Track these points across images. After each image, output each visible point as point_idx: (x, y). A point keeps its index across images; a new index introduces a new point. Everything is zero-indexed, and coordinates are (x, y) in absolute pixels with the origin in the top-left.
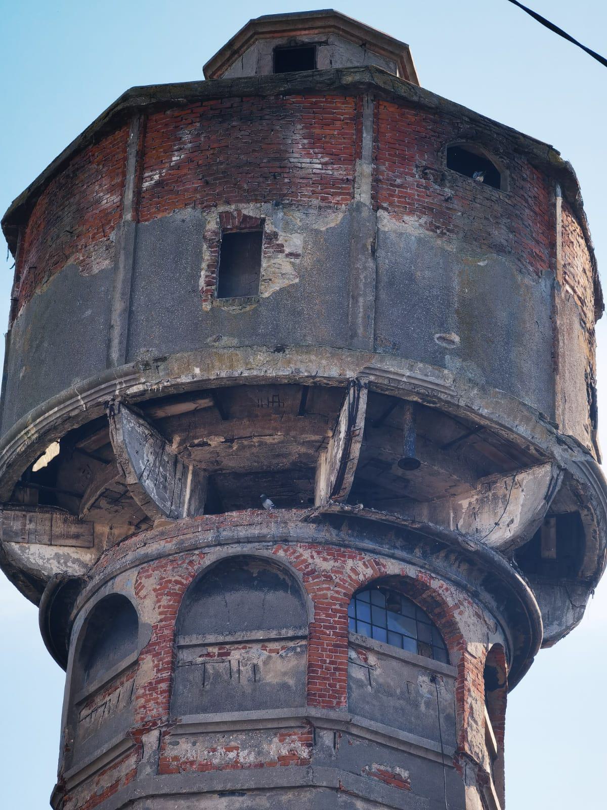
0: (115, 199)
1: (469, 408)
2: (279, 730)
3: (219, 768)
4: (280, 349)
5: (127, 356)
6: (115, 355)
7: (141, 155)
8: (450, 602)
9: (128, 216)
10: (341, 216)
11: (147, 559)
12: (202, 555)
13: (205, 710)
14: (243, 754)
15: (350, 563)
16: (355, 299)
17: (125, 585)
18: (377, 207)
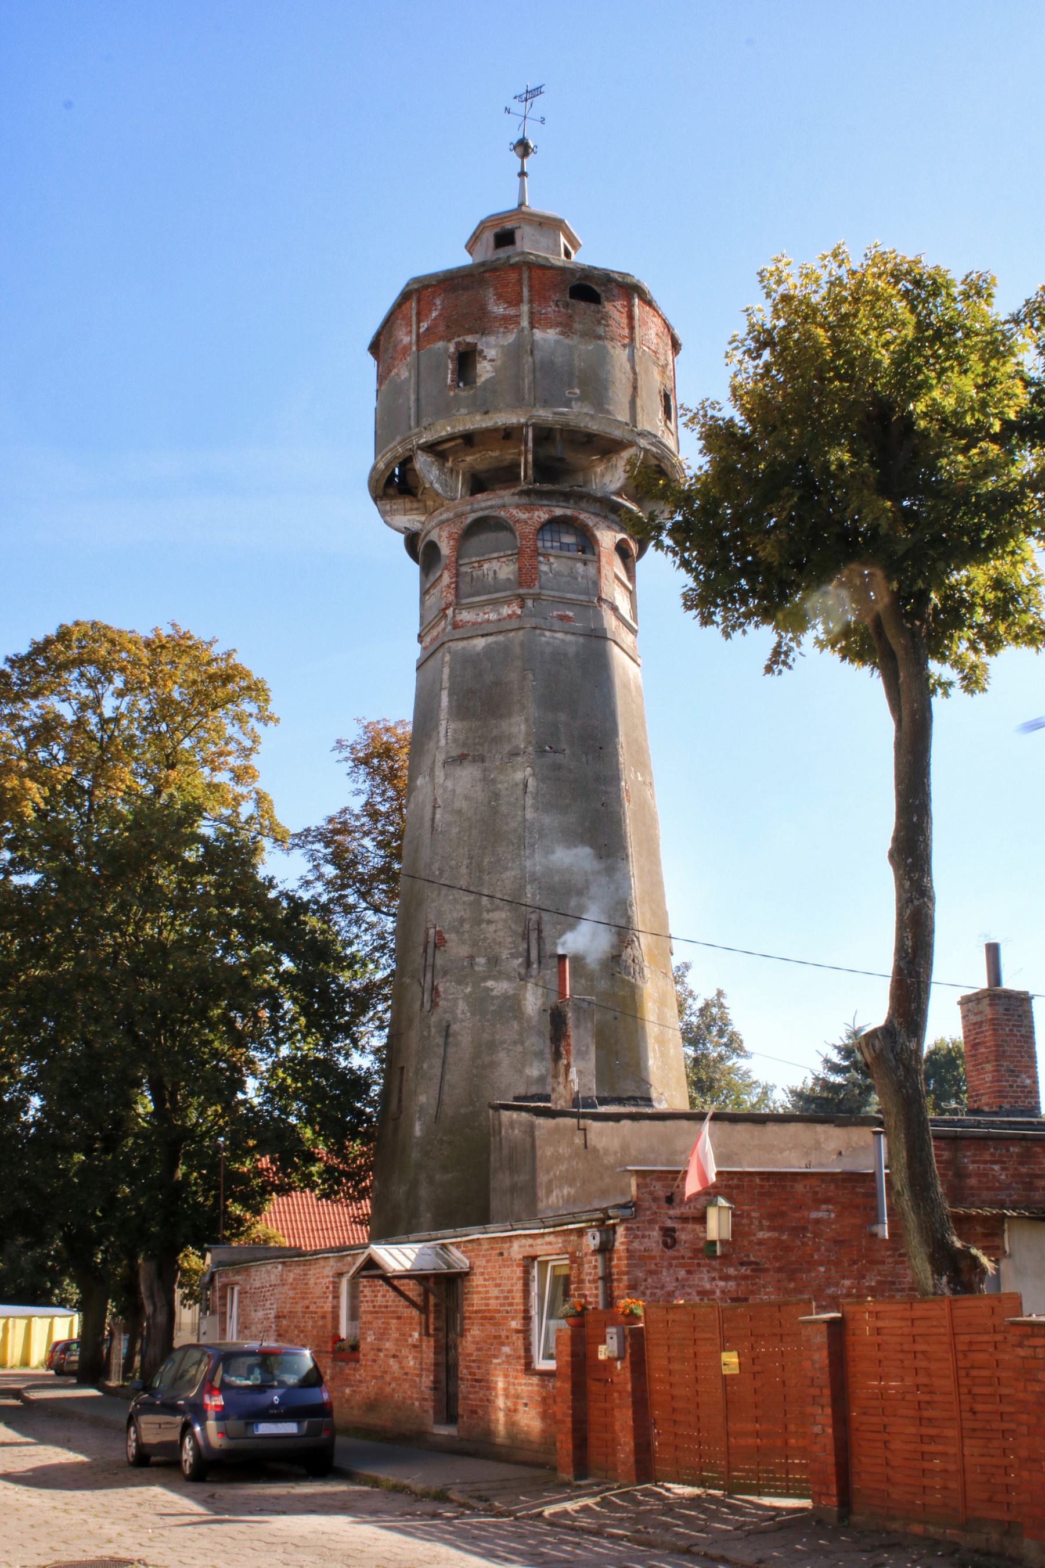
0: (409, 339)
1: (586, 427)
2: (508, 603)
3: (481, 624)
4: (486, 413)
5: (418, 423)
6: (413, 423)
7: (418, 314)
8: (591, 524)
9: (414, 348)
10: (514, 336)
11: (442, 522)
12: (466, 518)
13: (473, 595)
14: (491, 615)
15: (536, 513)
16: (523, 379)
17: (434, 536)
18: (532, 327)
